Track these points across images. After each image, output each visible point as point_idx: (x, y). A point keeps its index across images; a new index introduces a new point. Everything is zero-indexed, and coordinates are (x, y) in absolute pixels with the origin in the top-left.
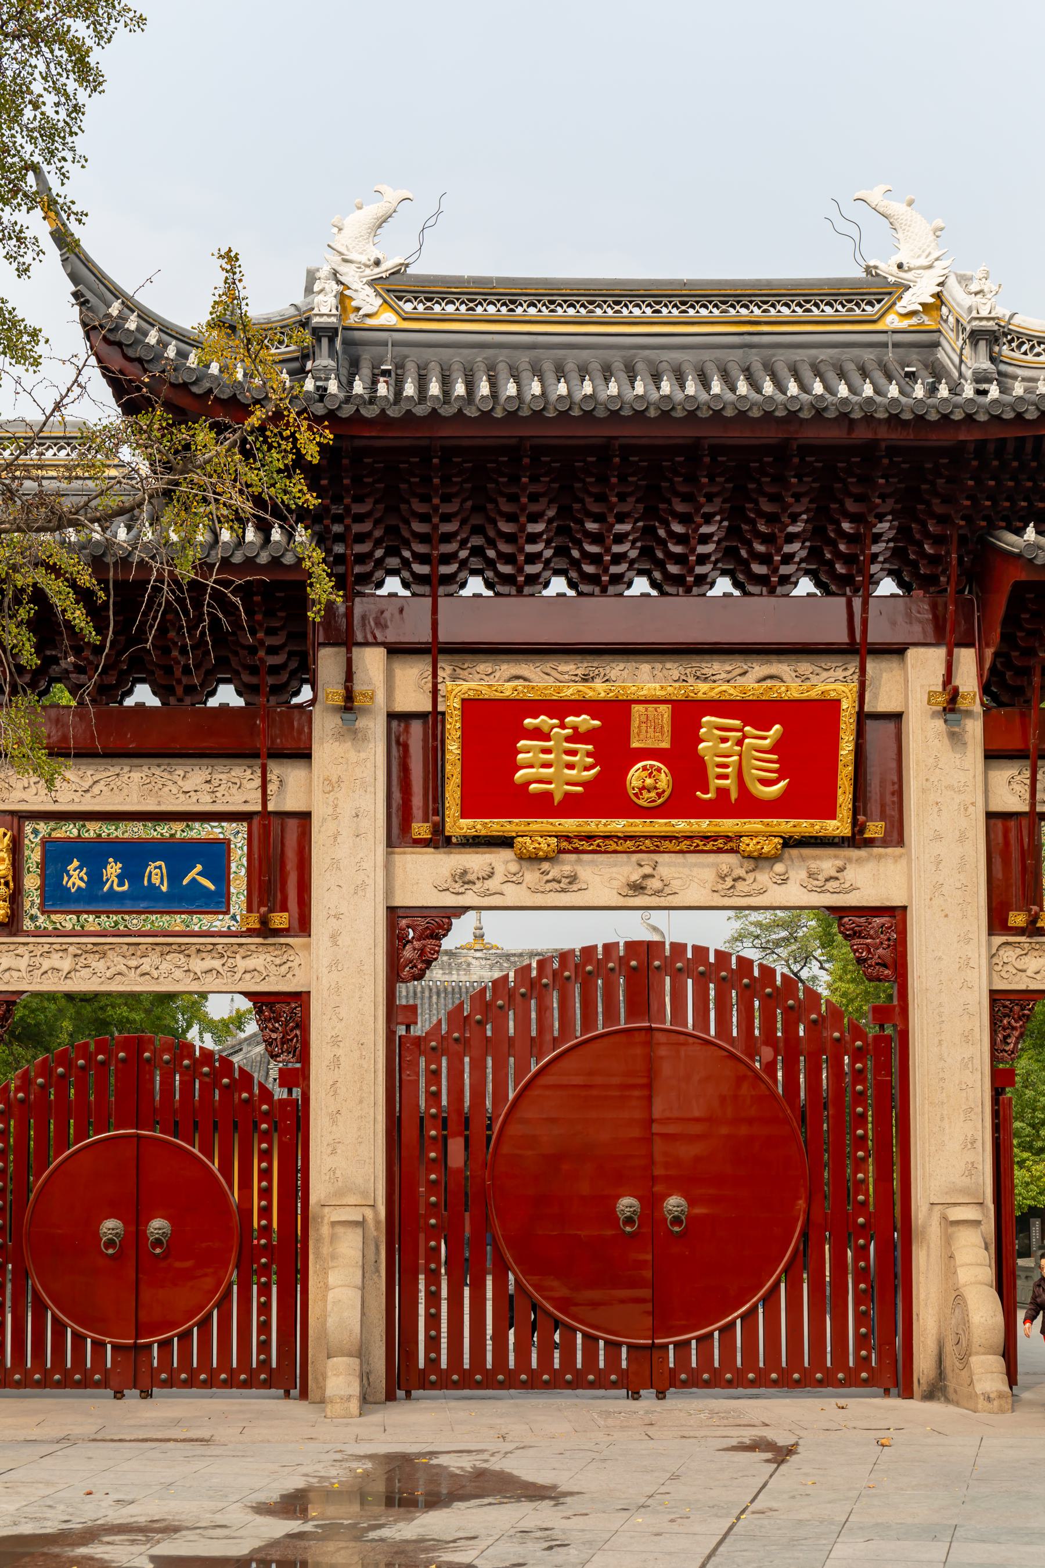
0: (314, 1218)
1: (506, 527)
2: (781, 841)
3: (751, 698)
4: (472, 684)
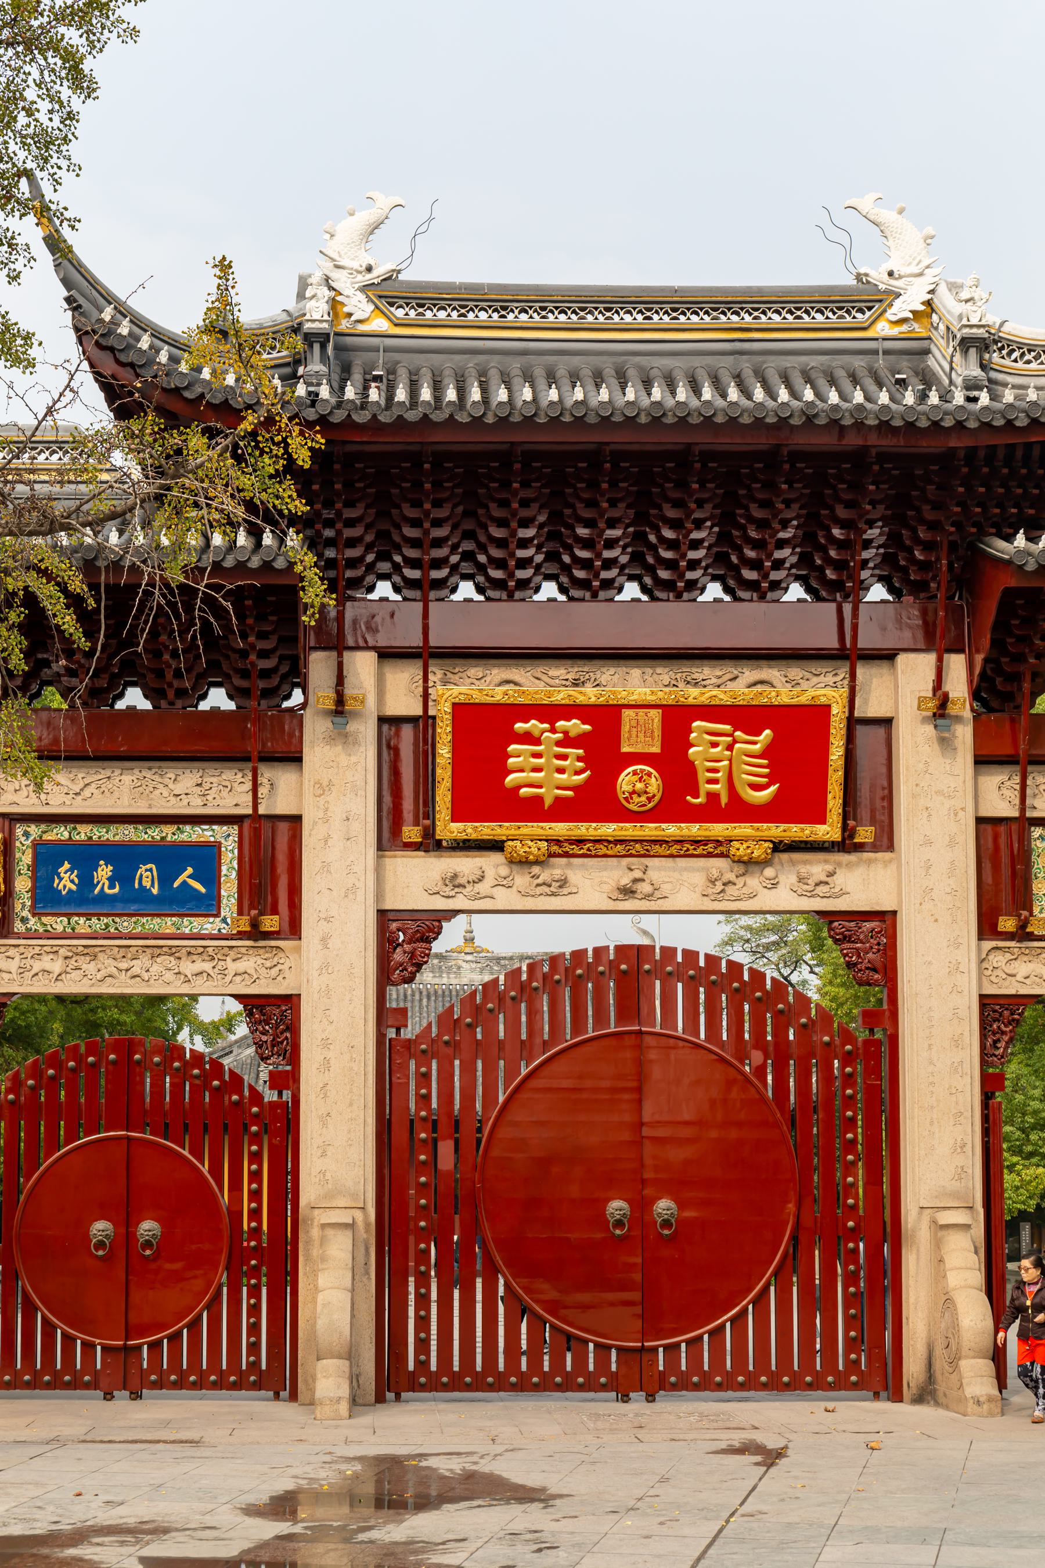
0: (304, 1220)
1: (497, 533)
3: (741, 703)
4: (463, 689)
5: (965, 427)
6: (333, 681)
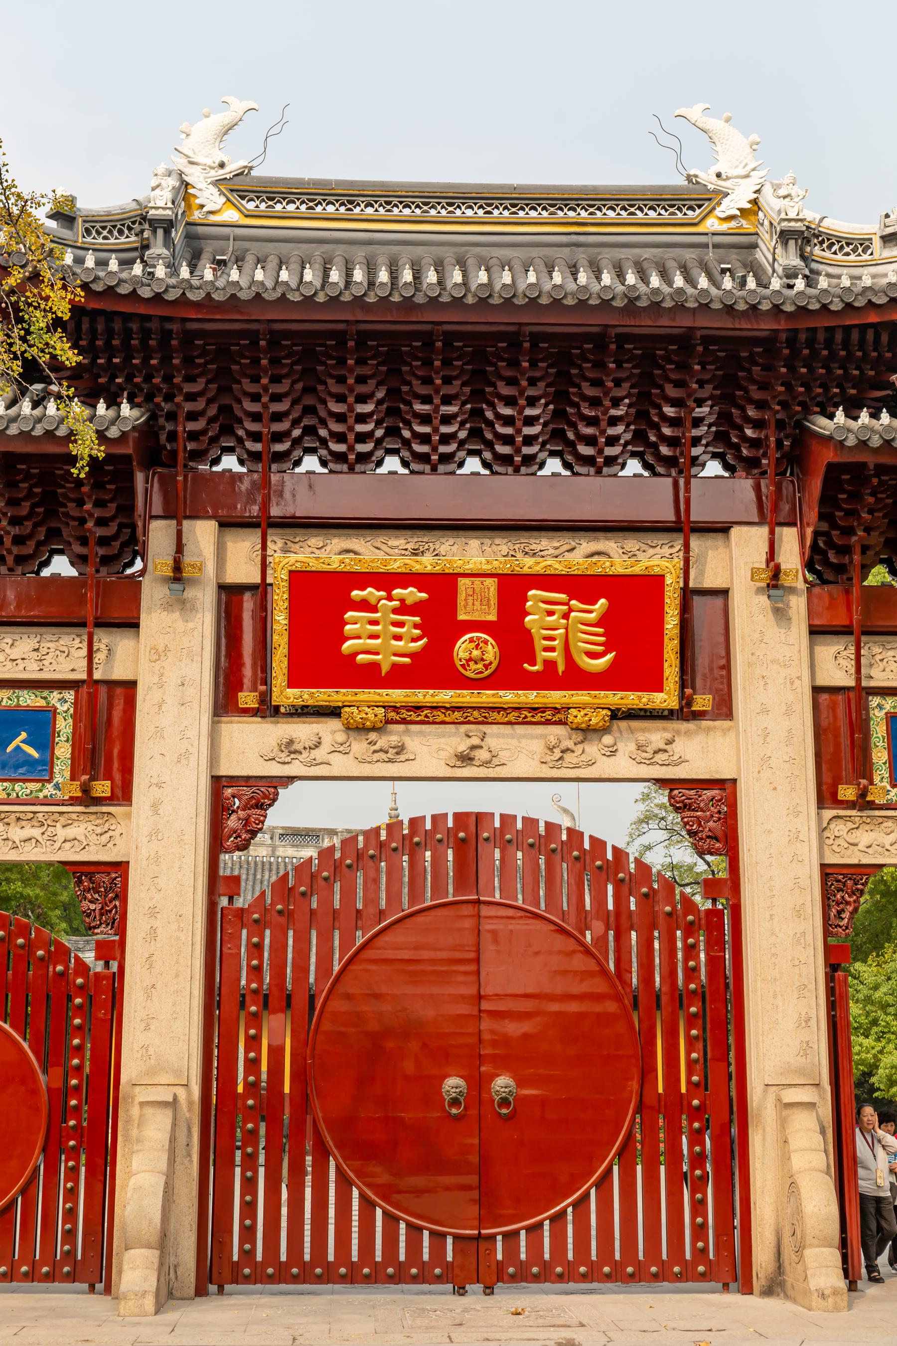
0: (124, 1098)
1: (336, 408)
3: (576, 573)
4: (300, 557)
6: (174, 548)
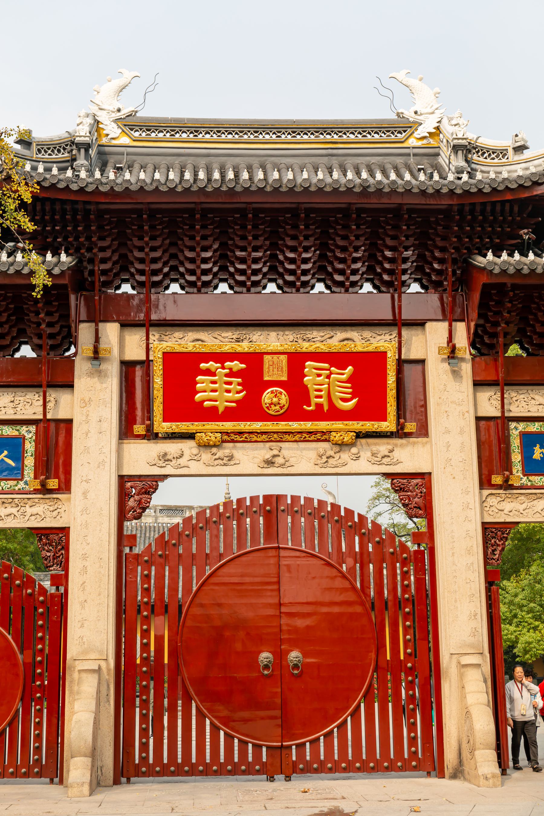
1: (190, 254)
2: (355, 434)
3: (334, 351)
4: (169, 344)
5: (455, 193)
